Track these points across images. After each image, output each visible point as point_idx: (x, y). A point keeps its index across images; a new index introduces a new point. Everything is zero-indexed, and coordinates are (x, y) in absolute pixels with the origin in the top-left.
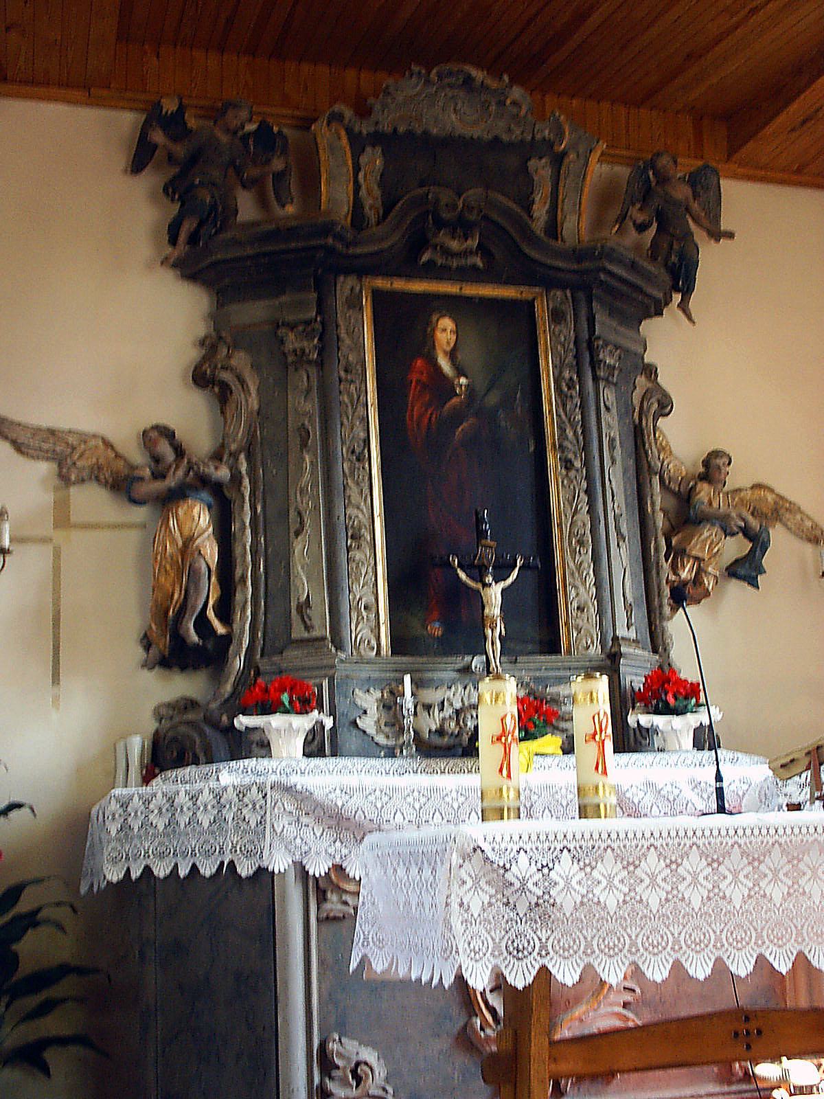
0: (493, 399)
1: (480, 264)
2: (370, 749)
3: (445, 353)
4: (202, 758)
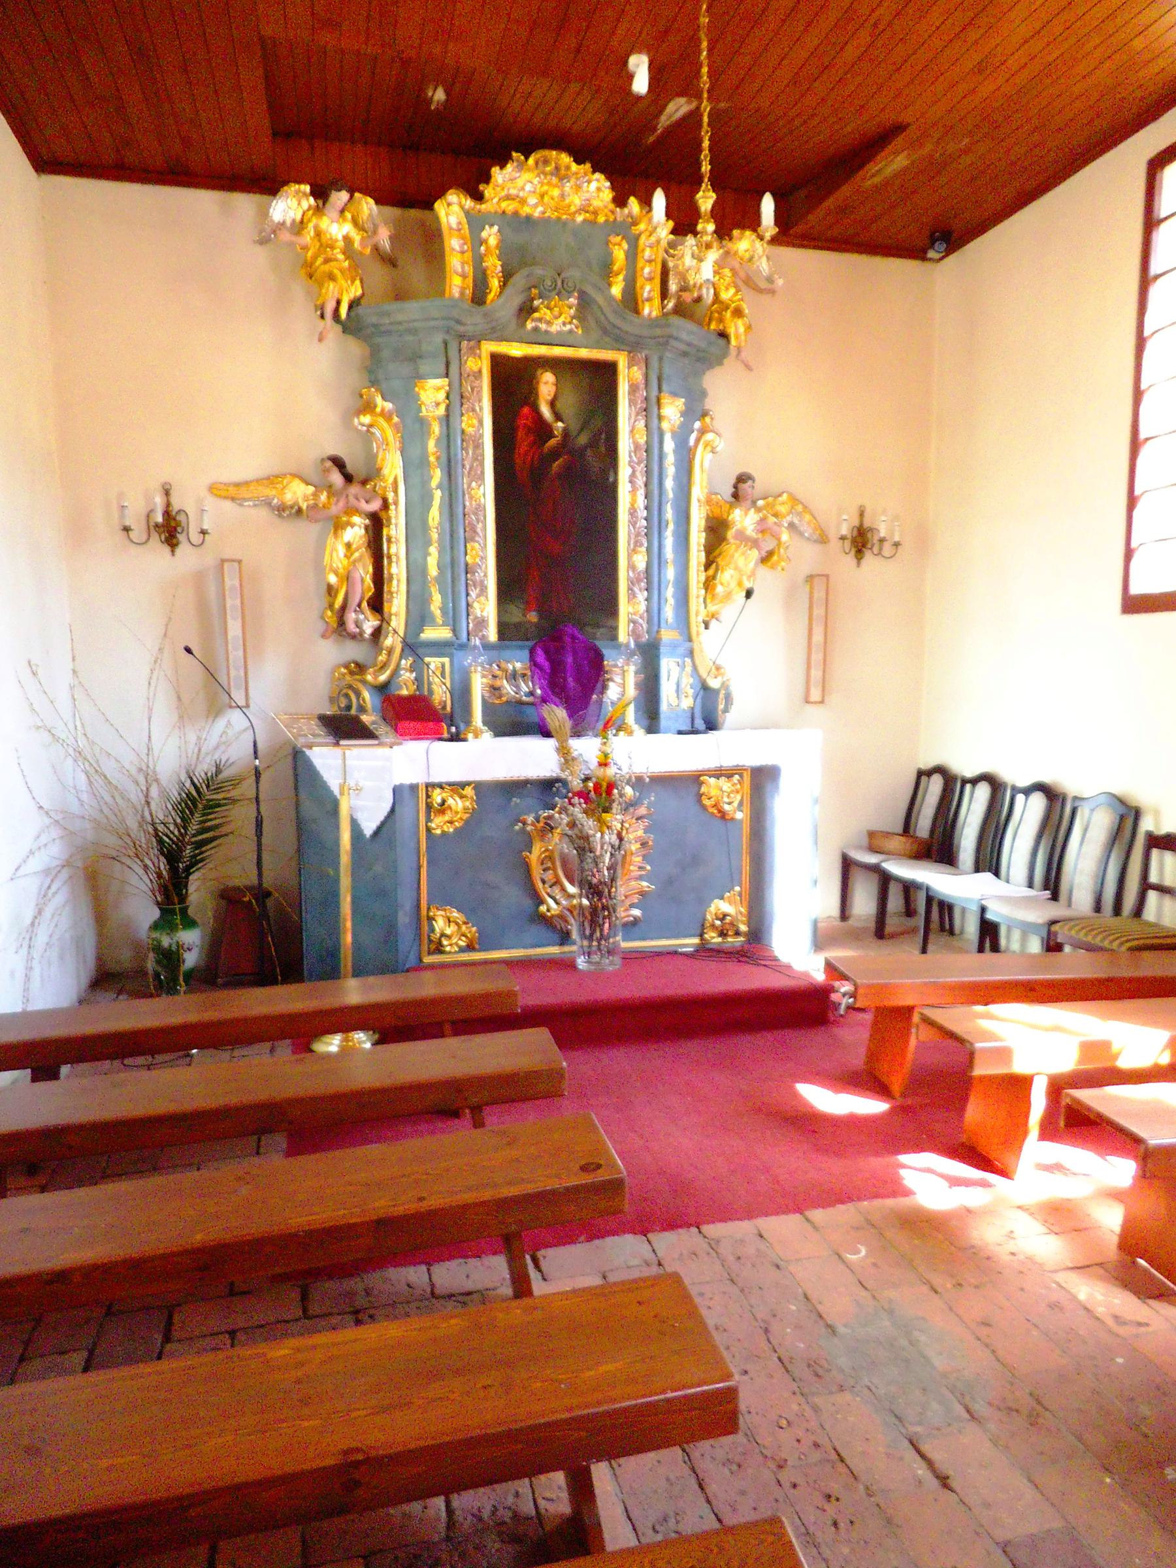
0: (583, 440)
1: (245, 899)
2: (898, 880)
3: (546, 401)
4: (730, 1407)
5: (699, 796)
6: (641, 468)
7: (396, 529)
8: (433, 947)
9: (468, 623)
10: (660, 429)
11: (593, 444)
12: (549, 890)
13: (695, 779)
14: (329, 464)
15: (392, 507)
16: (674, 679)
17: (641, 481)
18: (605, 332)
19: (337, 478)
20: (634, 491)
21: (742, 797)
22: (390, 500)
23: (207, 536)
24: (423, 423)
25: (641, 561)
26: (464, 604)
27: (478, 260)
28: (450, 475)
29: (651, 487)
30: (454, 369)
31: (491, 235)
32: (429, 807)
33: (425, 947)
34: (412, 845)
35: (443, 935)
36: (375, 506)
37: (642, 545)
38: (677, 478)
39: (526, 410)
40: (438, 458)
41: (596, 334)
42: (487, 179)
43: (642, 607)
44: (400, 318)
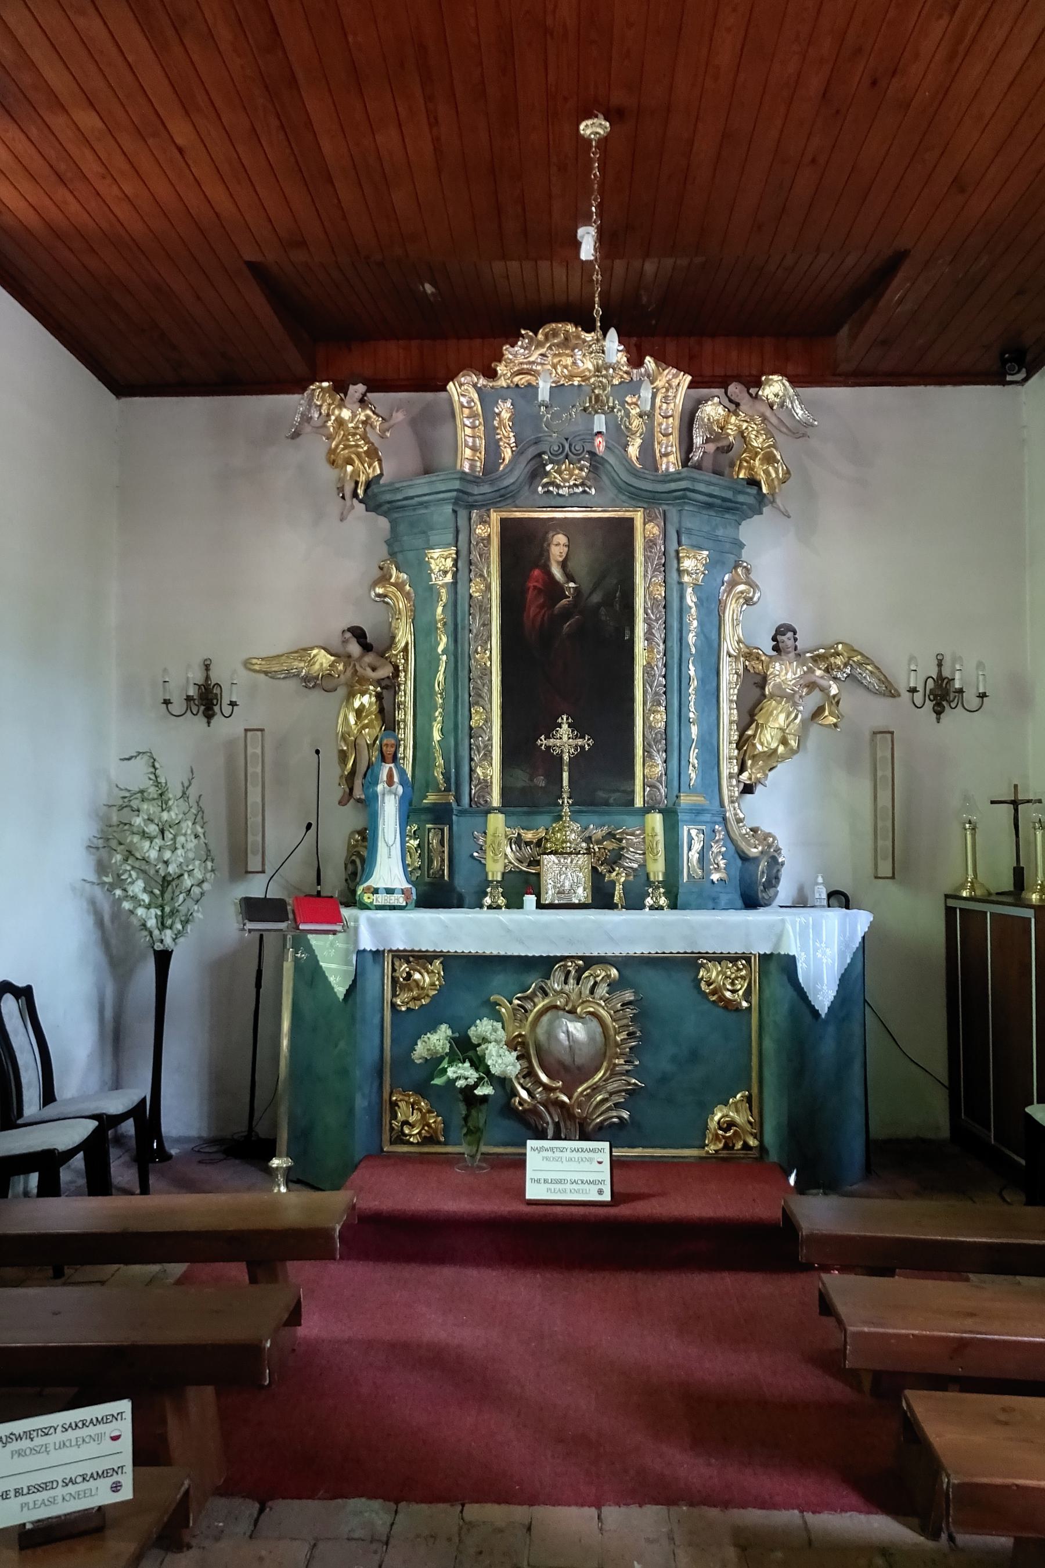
0: (596, 598)
5: (697, 982)
6: (658, 626)
7: (406, 695)
8: (394, 1135)
9: (471, 789)
10: (680, 583)
11: (608, 601)
12: (522, 1081)
13: (691, 963)
14: (348, 635)
15: (402, 674)
16: (697, 846)
17: (659, 636)
18: (620, 489)
19: (355, 648)
20: (650, 649)
21: (749, 985)
22: (401, 668)
23: (235, 707)
24: (432, 591)
25: (659, 719)
26: (466, 769)
27: (491, 432)
28: (456, 641)
29: (669, 644)
30: (463, 537)
31: (504, 410)
32: (394, 981)
33: (386, 1136)
34: (376, 1020)
35: (406, 1123)
36: (386, 671)
37: (660, 704)
38: (702, 633)
39: (536, 572)
40: (445, 624)
41: (611, 493)
42: (499, 357)
43: (660, 769)
44: (411, 493)
